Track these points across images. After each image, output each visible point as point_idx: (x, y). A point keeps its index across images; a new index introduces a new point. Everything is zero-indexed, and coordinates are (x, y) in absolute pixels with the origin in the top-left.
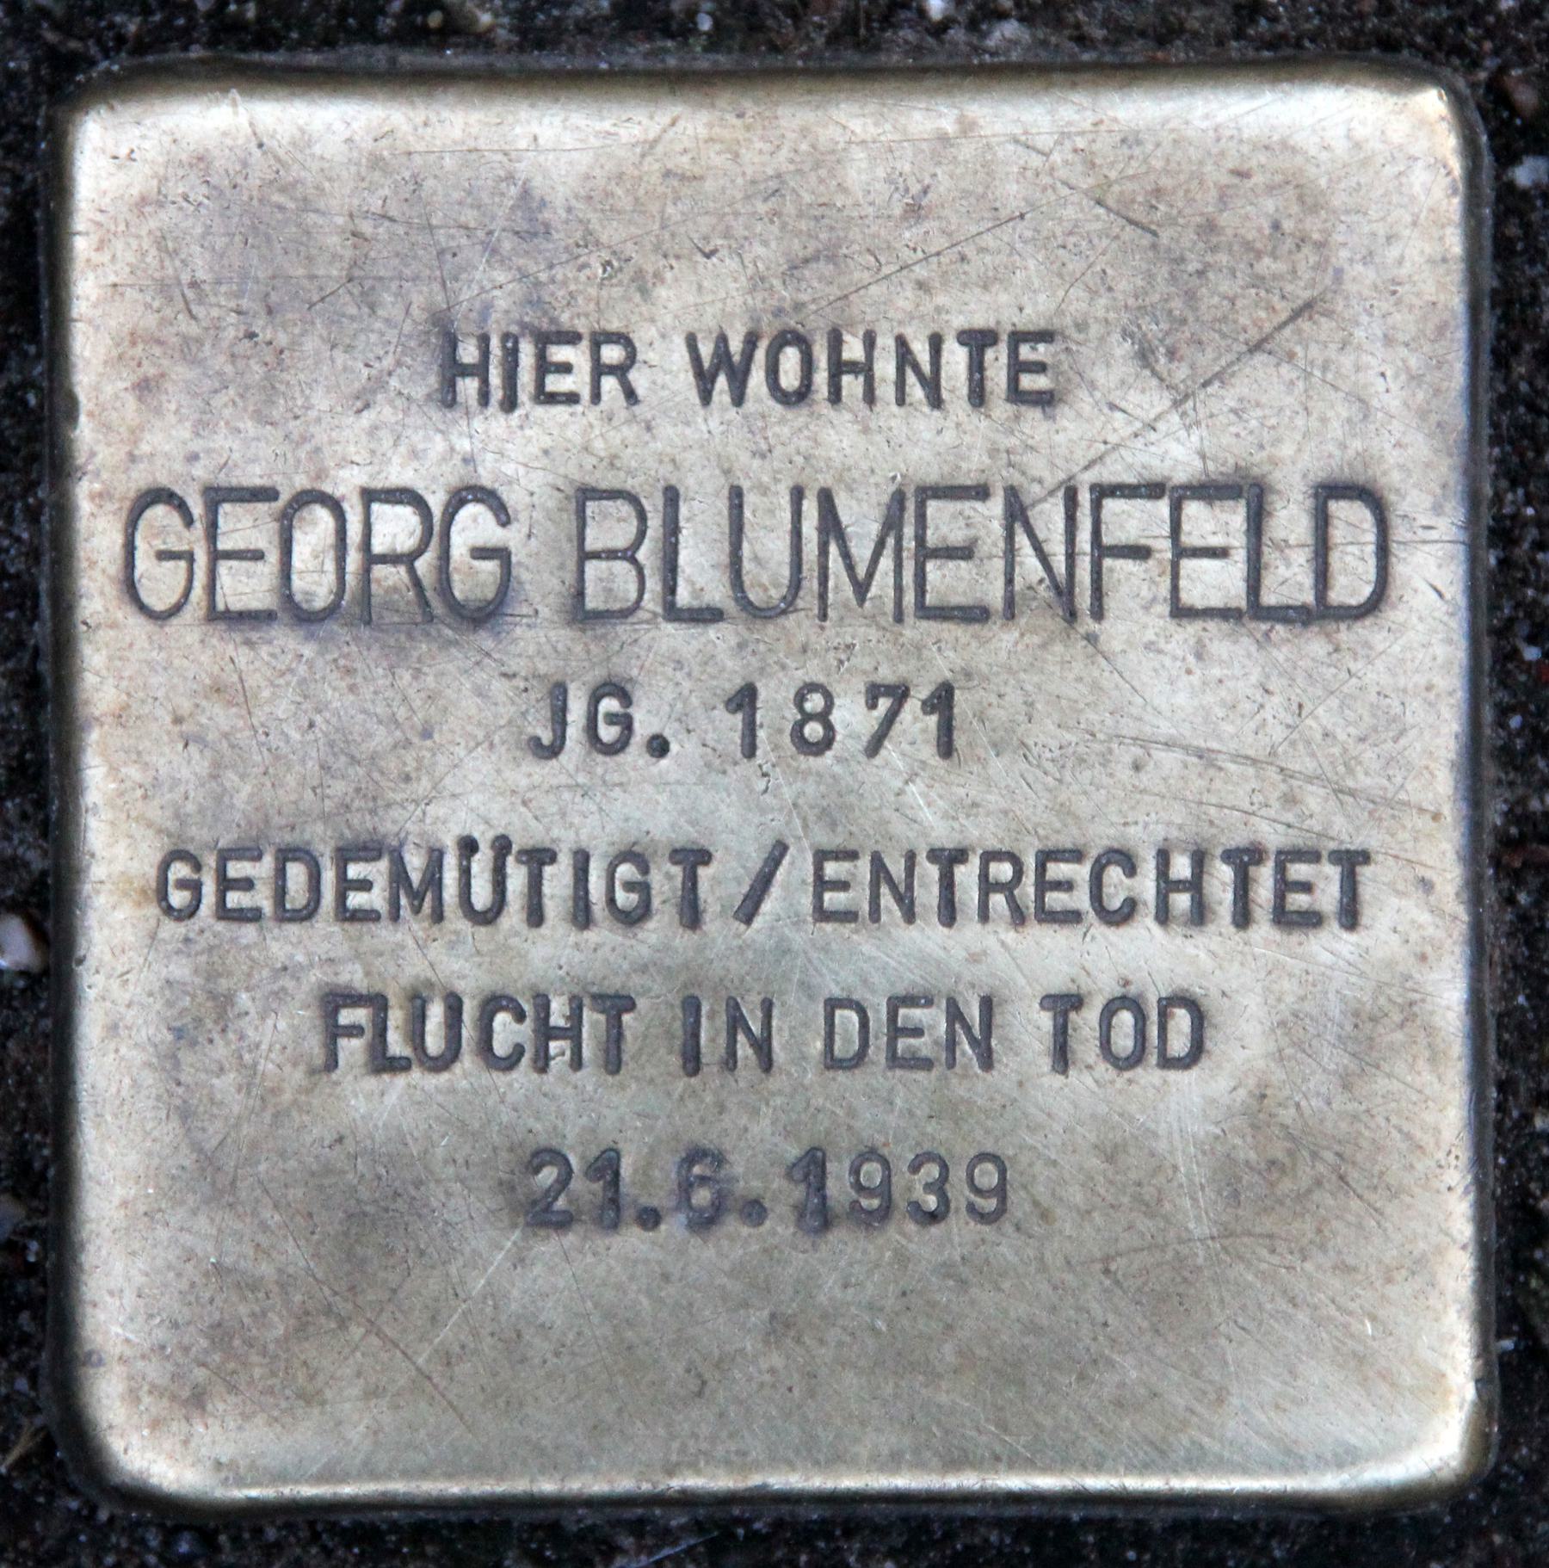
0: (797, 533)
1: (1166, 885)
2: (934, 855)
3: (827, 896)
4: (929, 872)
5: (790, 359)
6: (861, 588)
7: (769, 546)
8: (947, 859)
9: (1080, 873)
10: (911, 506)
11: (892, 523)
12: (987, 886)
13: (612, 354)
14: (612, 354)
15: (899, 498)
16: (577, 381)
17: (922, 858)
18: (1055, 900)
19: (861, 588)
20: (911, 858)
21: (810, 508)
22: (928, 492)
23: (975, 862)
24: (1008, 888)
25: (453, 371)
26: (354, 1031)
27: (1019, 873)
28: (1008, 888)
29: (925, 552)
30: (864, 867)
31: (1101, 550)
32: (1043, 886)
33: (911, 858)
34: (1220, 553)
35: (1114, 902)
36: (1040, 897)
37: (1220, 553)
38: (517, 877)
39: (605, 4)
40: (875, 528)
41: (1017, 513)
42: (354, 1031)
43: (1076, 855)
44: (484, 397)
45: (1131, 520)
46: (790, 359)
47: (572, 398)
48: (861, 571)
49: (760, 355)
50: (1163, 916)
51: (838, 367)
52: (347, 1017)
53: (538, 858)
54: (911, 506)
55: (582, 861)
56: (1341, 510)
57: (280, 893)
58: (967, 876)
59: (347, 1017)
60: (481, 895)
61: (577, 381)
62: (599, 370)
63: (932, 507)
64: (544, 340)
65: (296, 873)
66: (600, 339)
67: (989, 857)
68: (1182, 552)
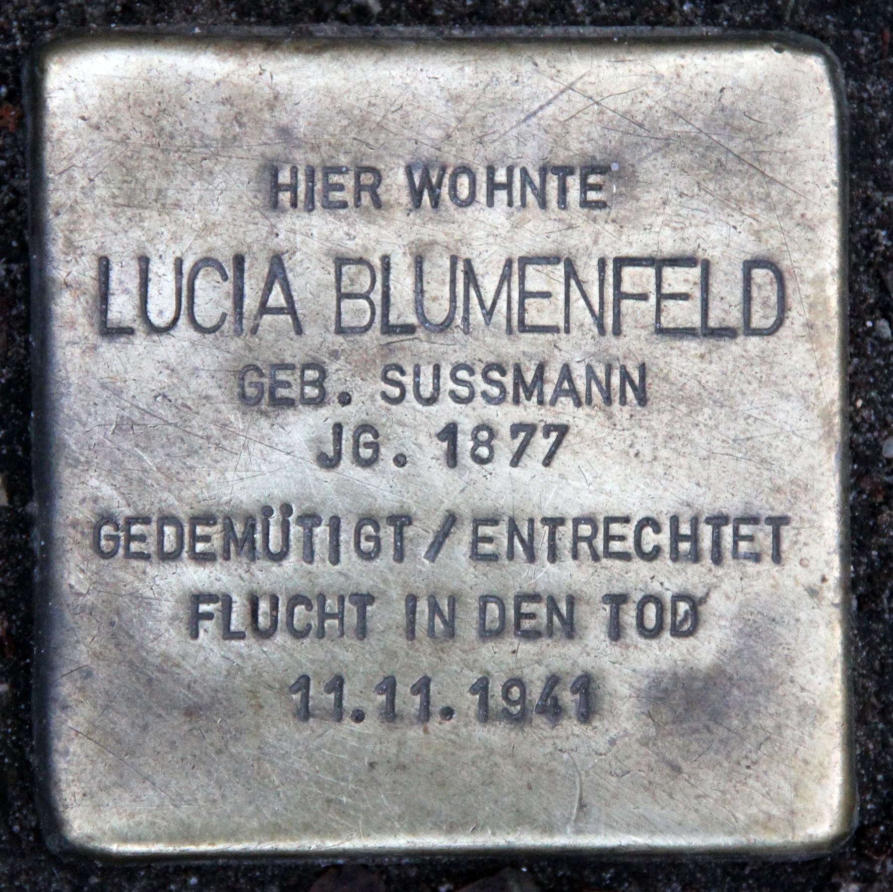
0: (453, 281)
1: (676, 537)
2: (545, 521)
3: (480, 545)
4: (543, 531)
5: (464, 181)
6: (489, 314)
7: (438, 290)
8: (555, 523)
9: (629, 530)
10: (516, 266)
11: (506, 277)
12: (577, 539)
13: (367, 179)
14: (367, 179)
15: (509, 263)
16: (347, 196)
17: (538, 525)
18: (616, 546)
19: (489, 314)
20: (531, 521)
21: (460, 266)
22: (525, 261)
23: (570, 524)
24: (589, 540)
25: (277, 188)
26: (209, 616)
27: (595, 530)
28: (589, 540)
29: (524, 295)
30: (503, 528)
31: (620, 296)
32: (608, 538)
33: (531, 521)
34: (685, 297)
35: (648, 548)
36: (606, 546)
37: (685, 297)
38: (295, 530)
39: (443, 890)
40: (496, 280)
41: (571, 273)
42: (209, 616)
43: (626, 520)
44: (294, 205)
45: (636, 279)
46: (464, 181)
47: (344, 205)
48: (488, 304)
49: (446, 181)
50: (676, 556)
51: (493, 186)
52: (204, 608)
53: (310, 519)
54: (516, 266)
55: (335, 525)
56: (760, 275)
57: (161, 543)
58: (565, 532)
59: (204, 608)
60: (274, 545)
61: (347, 196)
62: (359, 188)
63: (530, 270)
64: (329, 170)
65: (169, 530)
66: (361, 170)
67: (577, 522)
68: (661, 297)
